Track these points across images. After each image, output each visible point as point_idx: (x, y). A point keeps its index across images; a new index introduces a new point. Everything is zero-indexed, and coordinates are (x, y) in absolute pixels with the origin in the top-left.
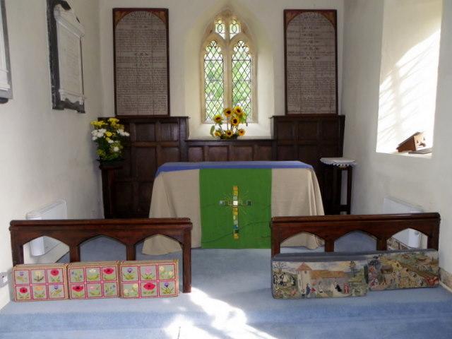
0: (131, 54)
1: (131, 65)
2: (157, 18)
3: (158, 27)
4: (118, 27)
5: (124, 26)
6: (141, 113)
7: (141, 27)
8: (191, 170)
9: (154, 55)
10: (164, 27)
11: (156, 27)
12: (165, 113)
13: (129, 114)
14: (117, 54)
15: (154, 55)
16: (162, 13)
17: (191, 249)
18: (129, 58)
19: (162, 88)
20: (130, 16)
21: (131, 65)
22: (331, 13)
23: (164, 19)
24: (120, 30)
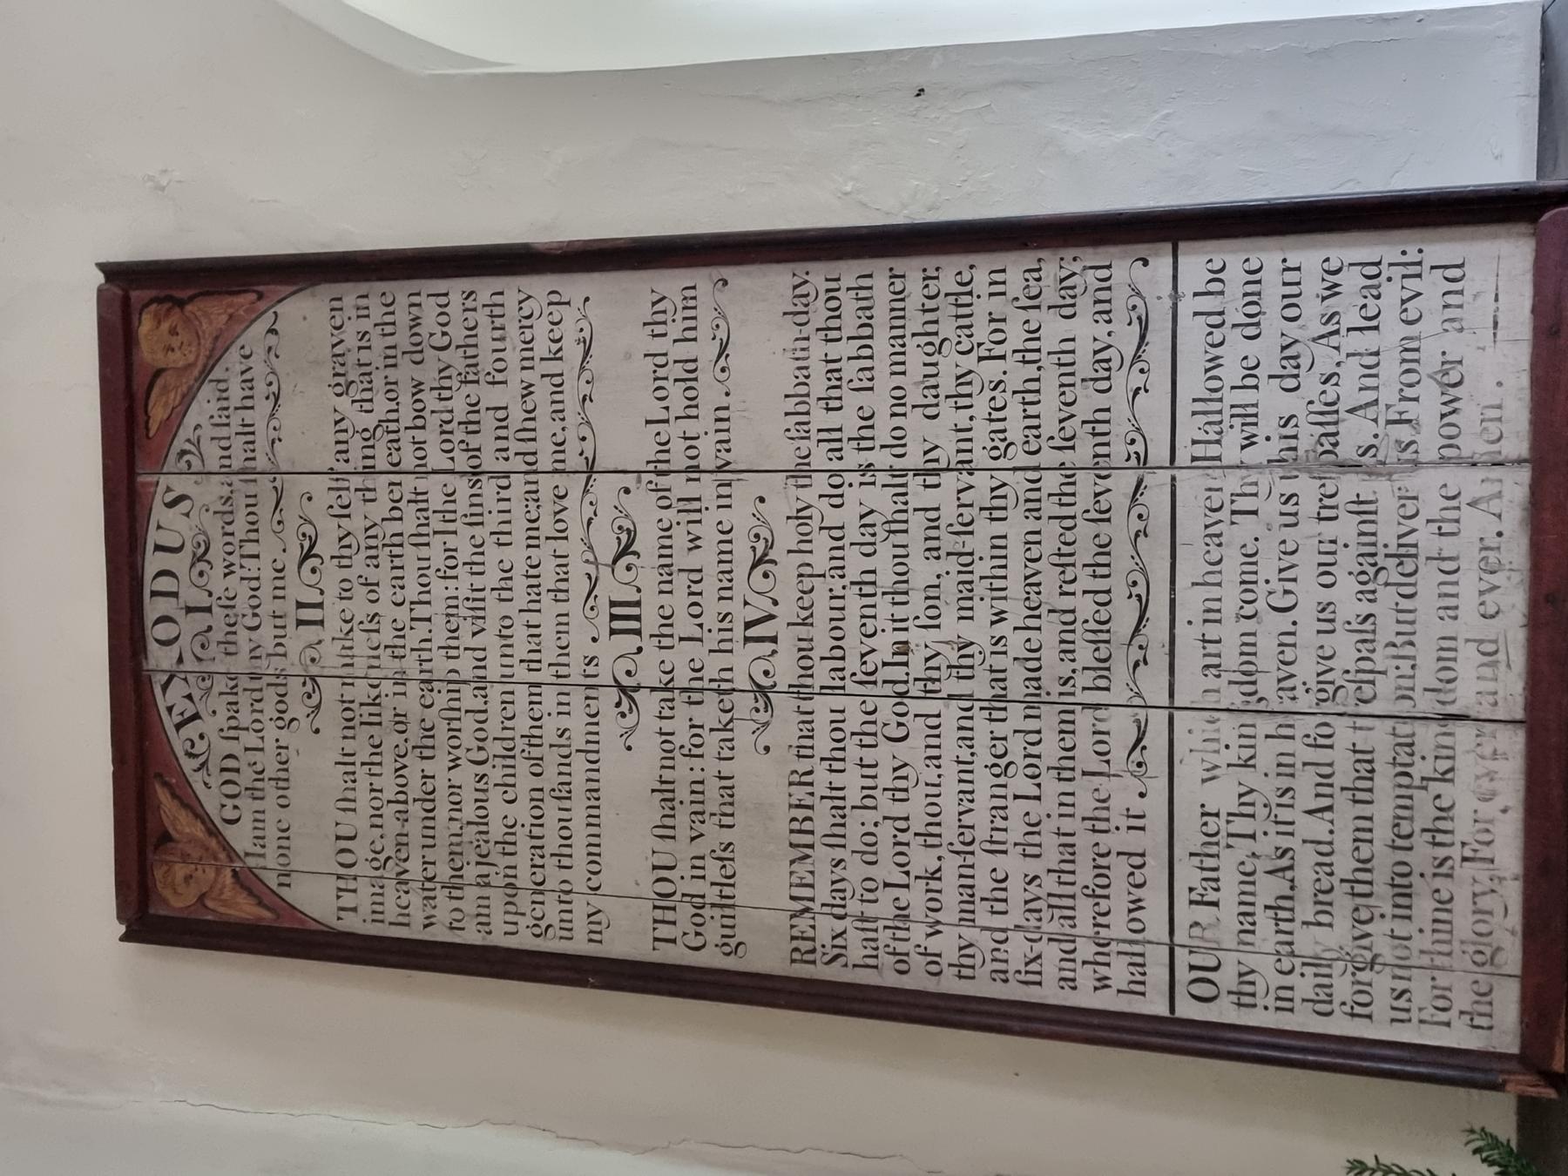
0: (629, 770)
1: (761, 776)
2: (202, 410)
3: (290, 389)
4: (315, 899)
5: (307, 825)
6: (1496, 679)
7: (308, 615)
8: (1012, 998)
9: (624, 443)
10: (304, 314)
11: (307, 423)
12: (1502, 267)
13: (1508, 851)
14: (628, 939)
15: (624, 443)
16: (152, 335)
17: (1531, 1059)
18: (665, 790)
19: (1085, 329)
20: (198, 734)
21: (761, 776)
22: (152, 335)
23: (212, 313)
24: (345, 875)
